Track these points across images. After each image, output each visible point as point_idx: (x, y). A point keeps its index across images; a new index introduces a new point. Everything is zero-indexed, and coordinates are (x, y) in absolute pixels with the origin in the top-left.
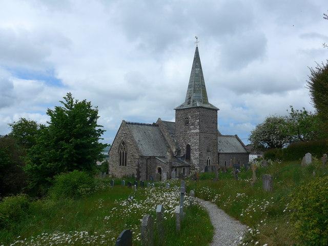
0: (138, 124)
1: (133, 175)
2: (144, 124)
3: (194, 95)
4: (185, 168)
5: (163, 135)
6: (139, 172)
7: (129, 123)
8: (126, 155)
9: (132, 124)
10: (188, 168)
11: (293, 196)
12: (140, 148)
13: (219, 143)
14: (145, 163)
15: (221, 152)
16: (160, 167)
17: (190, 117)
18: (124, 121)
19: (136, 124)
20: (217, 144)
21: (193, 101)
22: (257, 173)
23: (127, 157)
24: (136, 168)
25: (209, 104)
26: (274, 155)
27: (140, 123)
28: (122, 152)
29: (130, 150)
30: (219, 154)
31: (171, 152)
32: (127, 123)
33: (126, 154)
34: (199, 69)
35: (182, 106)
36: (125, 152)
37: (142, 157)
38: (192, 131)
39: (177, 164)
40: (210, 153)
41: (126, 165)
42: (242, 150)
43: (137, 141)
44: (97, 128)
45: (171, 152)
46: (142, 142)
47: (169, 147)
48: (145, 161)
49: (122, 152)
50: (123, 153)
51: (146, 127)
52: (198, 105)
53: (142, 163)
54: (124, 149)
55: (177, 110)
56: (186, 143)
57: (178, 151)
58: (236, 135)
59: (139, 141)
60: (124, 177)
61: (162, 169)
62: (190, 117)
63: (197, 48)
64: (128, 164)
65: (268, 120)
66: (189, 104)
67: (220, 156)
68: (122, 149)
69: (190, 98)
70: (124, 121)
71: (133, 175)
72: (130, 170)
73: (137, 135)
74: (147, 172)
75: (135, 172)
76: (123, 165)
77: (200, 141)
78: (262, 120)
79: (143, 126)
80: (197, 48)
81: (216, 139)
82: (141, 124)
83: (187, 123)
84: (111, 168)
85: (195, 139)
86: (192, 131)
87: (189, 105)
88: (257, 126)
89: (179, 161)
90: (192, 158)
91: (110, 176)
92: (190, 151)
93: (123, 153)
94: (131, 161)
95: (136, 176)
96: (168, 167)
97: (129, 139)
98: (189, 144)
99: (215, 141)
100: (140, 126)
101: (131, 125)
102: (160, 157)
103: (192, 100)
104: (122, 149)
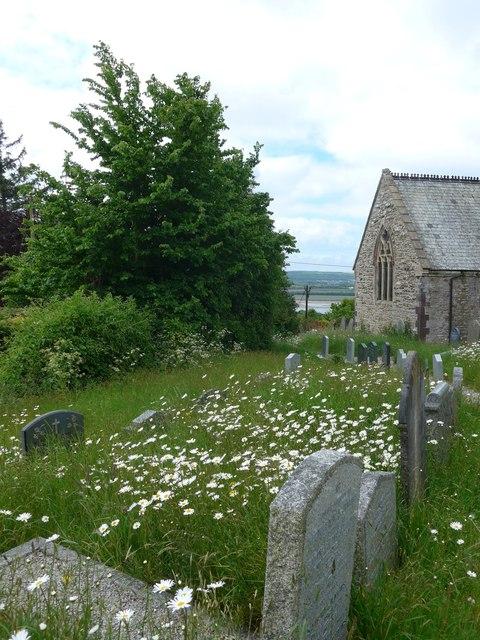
0: (435, 179)
1: (408, 325)
2: (455, 180)
6: (423, 318)
7: (405, 178)
8: (391, 266)
9: (415, 178)
11: (232, 178)
12: (431, 245)
18: (386, 172)
19: (425, 178)
22: (65, 418)
23: (394, 275)
24: (417, 304)
27: (441, 174)
28: (383, 260)
29: (404, 254)
32: (396, 177)
33: (392, 265)
36: (389, 260)
37: (433, 272)
43: (423, 226)
44: (250, 178)
46: (439, 229)
48: (443, 285)
49: (383, 260)
51: (462, 185)
54: (389, 252)
59: (430, 226)
60: (386, 331)
68: (383, 252)
70: (386, 172)
71: (408, 325)
72: (402, 312)
73: (424, 209)
74: (450, 318)
75: (414, 318)
76: (385, 298)
79: (450, 185)
82: (445, 180)
84: (359, 308)
91: (358, 329)
94: (402, 287)
95: (415, 329)
97: (400, 222)
100: (439, 185)
101: (409, 183)
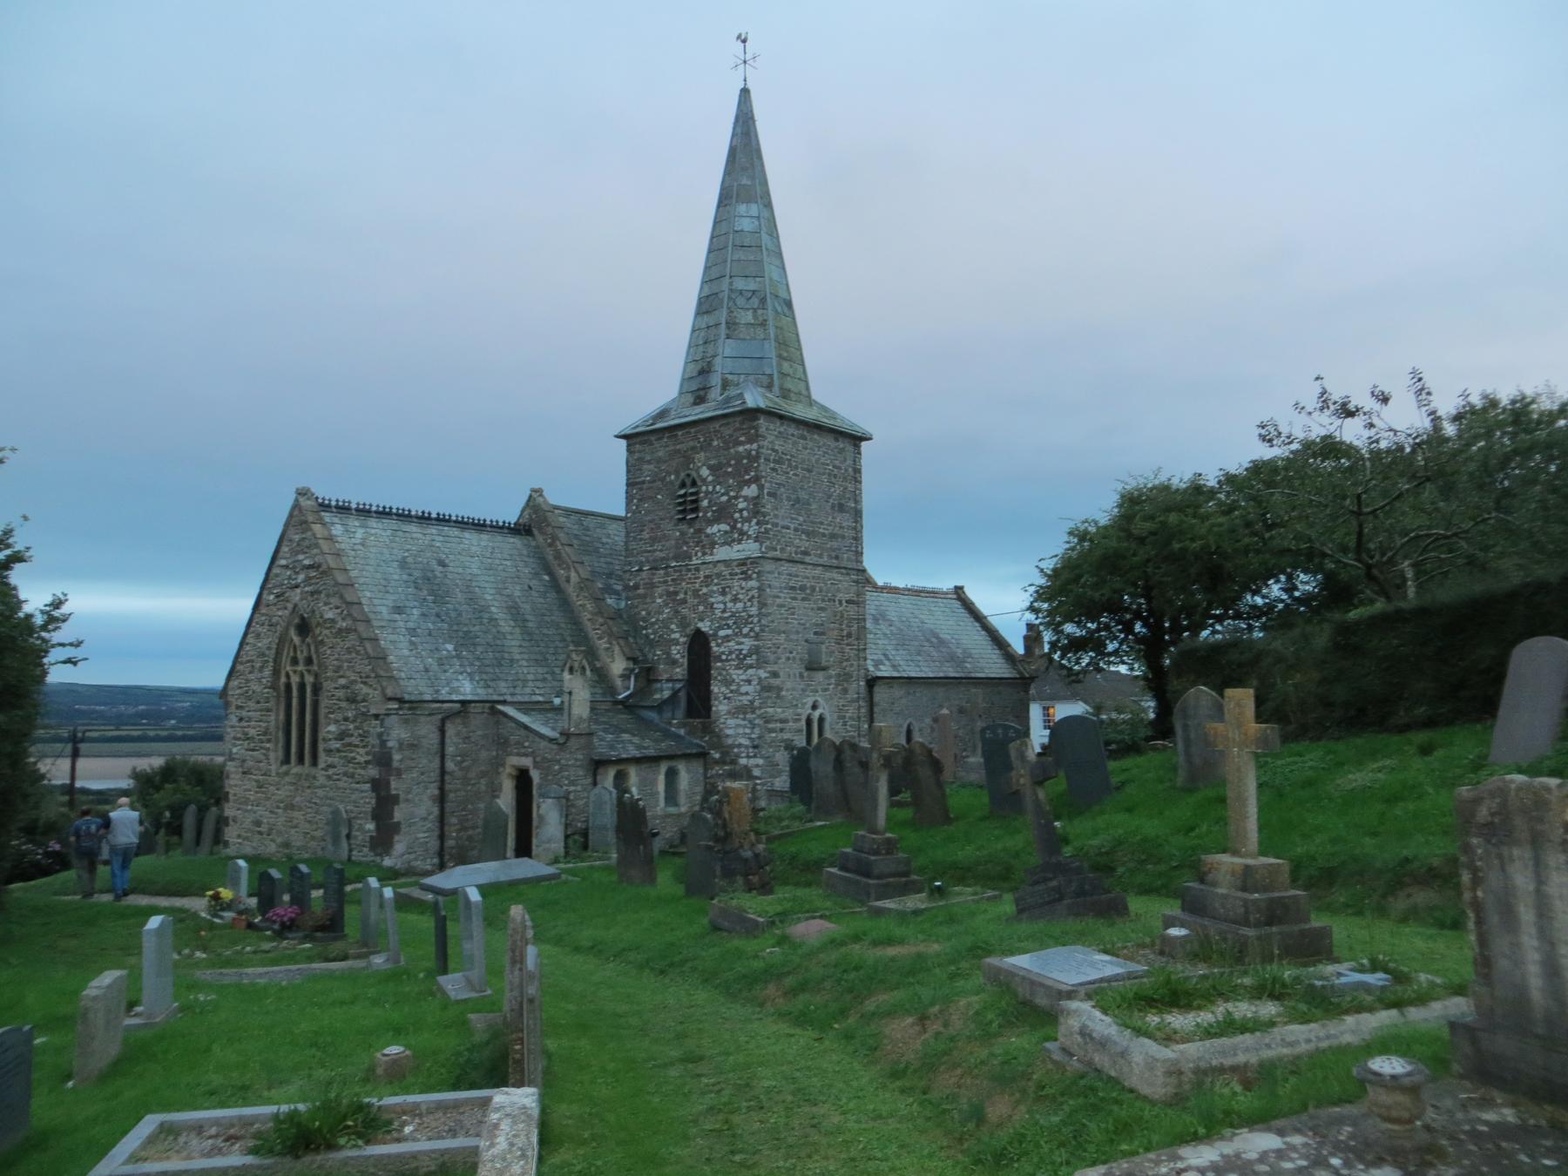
0: (404, 516)
3: (728, 348)
4: (682, 767)
5: (555, 586)
10: (697, 766)
13: (869, 625)
14: (434, 738)
15: (885, 671)
16: (526, 762)
17: (705, 472)
19: (384, 513)
20: (863, 629)
21: (725, 385)
23: (322, 711)
24: (373, 772)
25: (811, 403)
26: (245, 1088)
27: (416, 509)
28: (295, 679)
30: (872, 682)
31: (601, 677)
32: (324, 506)
33: (317, 689)
34: (754, 209)
35: (663, 414)
36: (309, 679)
38: (722, 553)
39: (631, 745)
40: (820, 676)
41: (314, 763)
42: (994, 666)
45: (601, 677)
47: (591, 654)
48: (427, 730)
49: (295, 679)
50: (302, 686)
51: (455, 532)
52: (751, 403)
53: (413, 746)
54: (309, 661)
55: (633, 439)
56: (684, 624)
57: (646, 674)
58: (959, 590)
61: (535, 775)
62: (705, 472)
63: (745, 93)
64: (329, 752)
65: (1132, 503)
66: (700, 399)
67: (881, 694)
69: (705, 371)
70: (303, 493)
74: (442, 799)
75: (366, 799)
77: (762, 605)
78: (1101, 508)
80: (745, 93)
81: (857, 602)
82: (424, 519)
83: (688, 508)
85: (735, 600)
86: (722, 553)
87: (698, 409)
88: (1123, 496)
89: (645, 726)
90: (720, 707)
92: (708, 668)
93: (302, 686)
96: (574, 758)
98: (705, 626)
99: (852, 609)
100: (413, 528)
101: (354, 522)
102: (526, 707)
103: (716, 380)
104: (295, 661)
